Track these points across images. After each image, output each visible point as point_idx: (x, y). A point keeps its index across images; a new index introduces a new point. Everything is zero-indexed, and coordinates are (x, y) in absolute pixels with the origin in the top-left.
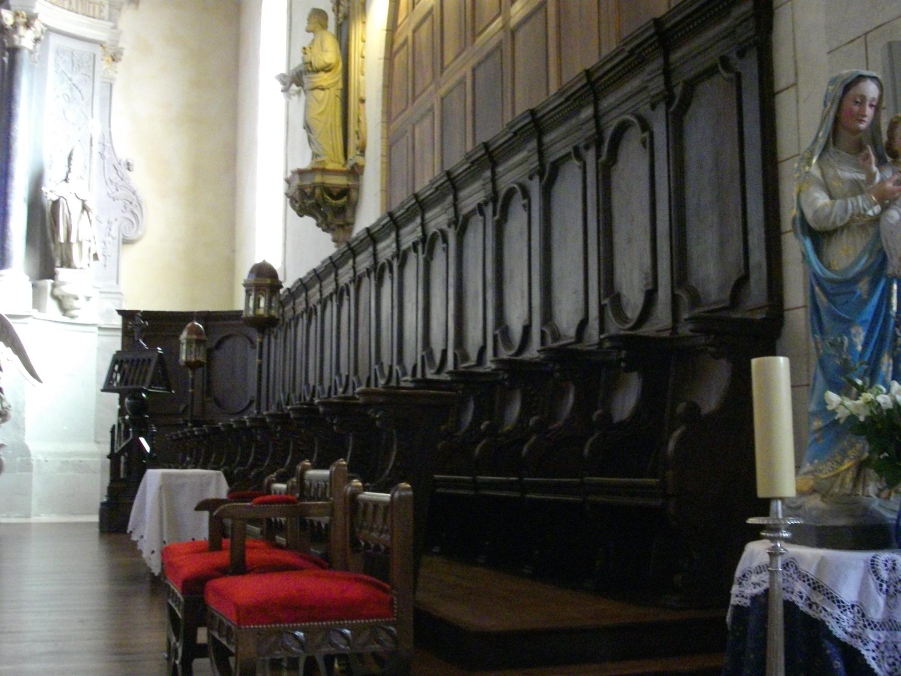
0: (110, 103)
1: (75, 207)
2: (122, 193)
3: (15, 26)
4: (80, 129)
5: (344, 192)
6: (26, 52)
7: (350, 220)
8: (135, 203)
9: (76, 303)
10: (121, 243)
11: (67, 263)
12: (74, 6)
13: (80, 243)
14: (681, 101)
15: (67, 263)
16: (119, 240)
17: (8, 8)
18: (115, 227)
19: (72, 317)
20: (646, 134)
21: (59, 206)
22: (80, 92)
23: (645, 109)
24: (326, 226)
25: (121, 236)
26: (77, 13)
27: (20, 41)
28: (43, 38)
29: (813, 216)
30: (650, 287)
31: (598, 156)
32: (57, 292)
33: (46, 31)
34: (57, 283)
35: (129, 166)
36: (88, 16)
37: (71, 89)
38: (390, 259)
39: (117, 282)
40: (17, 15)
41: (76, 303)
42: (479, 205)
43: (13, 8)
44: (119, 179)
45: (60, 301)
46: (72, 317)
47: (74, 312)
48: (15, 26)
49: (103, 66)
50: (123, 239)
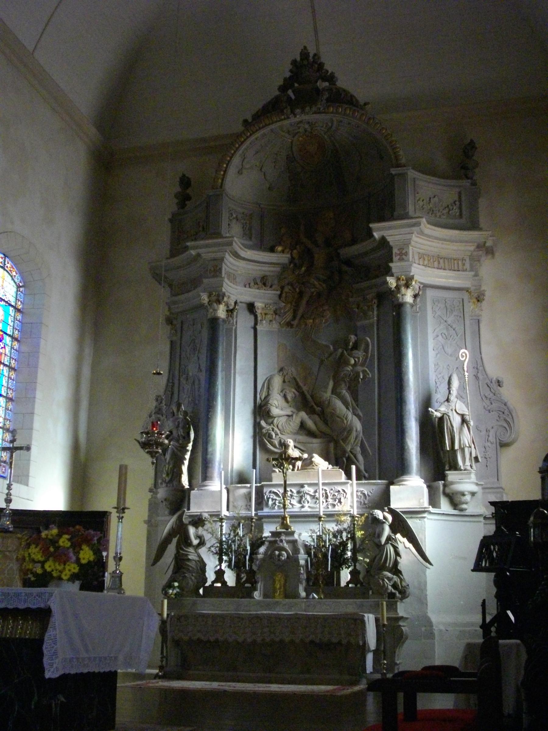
1: (456, 421)
6: (408, 306)
8: (506, 412)
11: (455, 467)
13: (462, 450)
15: (455, 467)
17: (392, 275)
18: (492, 433)
25: (498, 441)
26: (444, 269)
27: (403, 298)
32: (448, 490)
35: (499, 383)
37: (447, 329)
40: (398, 279)
43: (395, 275)
44: (492, 395)
46: (462, 510)
47: (464, 506)
49: (470, 307)
50: (500, 443)
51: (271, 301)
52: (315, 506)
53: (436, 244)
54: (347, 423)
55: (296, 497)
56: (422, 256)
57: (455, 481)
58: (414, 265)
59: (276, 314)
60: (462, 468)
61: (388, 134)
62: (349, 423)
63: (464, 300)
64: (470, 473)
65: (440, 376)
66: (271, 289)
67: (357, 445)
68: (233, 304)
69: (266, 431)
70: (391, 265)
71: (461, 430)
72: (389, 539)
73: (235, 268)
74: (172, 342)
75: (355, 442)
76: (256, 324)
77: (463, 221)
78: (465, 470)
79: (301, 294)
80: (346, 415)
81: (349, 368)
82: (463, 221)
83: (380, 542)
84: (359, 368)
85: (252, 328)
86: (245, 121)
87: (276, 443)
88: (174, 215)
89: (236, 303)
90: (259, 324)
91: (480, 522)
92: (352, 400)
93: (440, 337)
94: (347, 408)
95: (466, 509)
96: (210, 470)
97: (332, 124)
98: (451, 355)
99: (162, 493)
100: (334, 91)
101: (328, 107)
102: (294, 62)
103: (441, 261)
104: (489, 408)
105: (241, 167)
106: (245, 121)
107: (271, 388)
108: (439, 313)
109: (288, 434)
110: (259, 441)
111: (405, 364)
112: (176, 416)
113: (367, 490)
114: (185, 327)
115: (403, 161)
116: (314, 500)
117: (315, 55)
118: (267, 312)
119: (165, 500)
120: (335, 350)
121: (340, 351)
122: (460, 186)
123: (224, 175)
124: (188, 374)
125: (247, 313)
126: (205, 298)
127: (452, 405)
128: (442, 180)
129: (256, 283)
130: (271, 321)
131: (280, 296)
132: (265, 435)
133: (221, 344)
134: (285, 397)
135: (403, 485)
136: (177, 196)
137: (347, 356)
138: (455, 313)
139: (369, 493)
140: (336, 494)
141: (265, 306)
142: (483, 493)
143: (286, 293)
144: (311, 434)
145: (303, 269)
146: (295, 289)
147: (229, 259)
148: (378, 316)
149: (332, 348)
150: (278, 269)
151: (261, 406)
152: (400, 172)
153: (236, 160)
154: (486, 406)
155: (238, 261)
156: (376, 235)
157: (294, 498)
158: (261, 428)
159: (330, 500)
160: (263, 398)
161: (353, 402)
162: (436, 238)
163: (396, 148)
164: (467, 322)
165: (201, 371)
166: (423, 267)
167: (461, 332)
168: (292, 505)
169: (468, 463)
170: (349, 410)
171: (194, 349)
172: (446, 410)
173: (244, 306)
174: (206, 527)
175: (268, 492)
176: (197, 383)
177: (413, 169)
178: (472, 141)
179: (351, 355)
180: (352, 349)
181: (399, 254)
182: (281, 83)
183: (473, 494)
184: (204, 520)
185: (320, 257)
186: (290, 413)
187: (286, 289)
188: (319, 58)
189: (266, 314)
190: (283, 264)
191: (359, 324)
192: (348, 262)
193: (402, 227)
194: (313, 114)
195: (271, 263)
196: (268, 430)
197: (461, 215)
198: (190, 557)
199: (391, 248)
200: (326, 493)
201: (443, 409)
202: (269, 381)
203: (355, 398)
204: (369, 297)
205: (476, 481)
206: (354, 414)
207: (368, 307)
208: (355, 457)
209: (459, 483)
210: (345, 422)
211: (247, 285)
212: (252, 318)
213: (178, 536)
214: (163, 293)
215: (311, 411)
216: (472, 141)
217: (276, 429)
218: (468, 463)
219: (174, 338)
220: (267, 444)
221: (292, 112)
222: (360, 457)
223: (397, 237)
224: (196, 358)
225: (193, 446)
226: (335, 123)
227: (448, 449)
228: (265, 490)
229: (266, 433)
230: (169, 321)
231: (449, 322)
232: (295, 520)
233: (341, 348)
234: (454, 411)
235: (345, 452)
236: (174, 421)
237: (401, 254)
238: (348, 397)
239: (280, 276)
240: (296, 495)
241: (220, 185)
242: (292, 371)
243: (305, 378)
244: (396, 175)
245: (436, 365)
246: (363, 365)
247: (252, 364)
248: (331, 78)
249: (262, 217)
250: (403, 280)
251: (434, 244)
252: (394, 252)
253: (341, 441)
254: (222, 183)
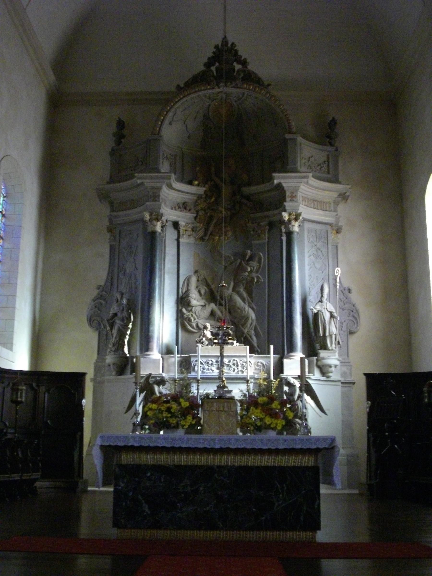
0: (337, 255)
1: (327, 316)
2: (347, 306)
3: (289, 221)
4: (322, 272)
6: (296, 233)
8: (354, 311)
9: (331, 369)
10: (348, 333)
11: (324, 347)
12: (316, 206)
13: (331, 336)
15: (324, 347)
16: (347, 333)
17: (285, 211)
18: (345, 324)
21: (318, 316)
22: (321, 252)
25: (348, 330)
26: (318, 209)
27: (293, 228)
28: (301, 224)
29: (243, 59)
32: (319, 363)
33: (303, 220)
34: (319, 358)
35: (349, 291)
36: (323, 210)
37: (317, 251)
39: (348, 356)
40: (290, 214)
41: (331, 369)
43: (287, 211)
44: (345, 298)
46: (328, 377)
48: (289, 221)
49: (332, 236)
50: (350, 332)
51: (190, 222)
52: (229, 371)
53: (315, 191)
54: (245, 312)
55: (215, 365)
56: (304, 199)
57: (325, 357)
58: (301, 205)
59: (193, 231)
60: (330, 348)
61: (284, 109)
62: (246, 313)
63: (328, 231)
64: (335, 352)
65: (311, 284)
66: (189, 212)
67: (252, 329)
68: (165, 222)
69: (187, 316)
70: (285, 203)
71: (330, 323)
72: (299, 397)
73: (166, 195)
74: (111, 246)
75: (250, 327)
78: (332, 350)
79: (211, 218)
80: (244, 307)
81: (247, 274)
83: (294, 399)
84: (254, 275)
85: (176, 240)
86: (178, 86)
87: (194, 325)
88: (113, 150)
89: (167, 221)
90: (181, 237)
91: (339, 385)
92: (248, 296)
93: (312, 256)
94: (245, 303)
95: (331, 377)
96: (151, 344)
97: (243, 96)
98: (319, 270)
99: (110, 359)
100: (247, 72)
102: (216, 47)
104: (343, 307)
105: (171, 120)
106: (178, 86)
107: (190, 285)
108: (311, 239)
109: (203, 319)
110: (181, 323)
111: (294, 275)
112: (119, 302)
113: (265, 361)
115: (294, 130)
116: (229, 368)
118: (187, 229)
119: (114, 364)
120: (235, 260)
121: (239, 261)
124: (125, 271)
126: (147, 216)
127: (324, 304)
129: (179, 207)
130: (189, 236)
131: (196, 218)
133: (158, 251)
134: (199, 292)
135: (292, 359)
136: (114, 135)
137: (245, 265)
138: (322, 240)
139: (267, 364)
140: (244, 364)
141: (186, 225)
142: (341, 366)
143: (200, 216)
146: (207, 214)
147: (165, 189)
148: (268, 238)
149: (232, 258)
150: (195, 198)
151: (182, 298)
152: (292, 137)
153: (170, 114)
154: (341, 306)
155: (168, 190)
156: (276, 182)
157: (213, 366)
158: (183, 314)
159: (240, 368)
160: (184, 292)
161: (249, 299)
162: (317, 188)
163: (290, 120)
164: (330, 246)
165: (137, 269)
166: (305, 207)
167: (325, 254)
168: (213, 371)
169: (334, 345)
170: (246, 304)
172: (321, 308)
173: (171, 223)
174: (165, 386)
175: (195, 360)
177: (301, 136)
178: (333, 118)
179: (248, 265)
180: (248, 260)
181: (291, 197)
182: (206, 61)
183: (336, 366)
184: (166, 381)
186: (203, 304)
187: (200, 213)
188: (235, 46)
189: (186, 230)
190: (199, 195)
191: (253, 242)
192: (248, 198)
193: (295, 177)
194: (232, 87)
195: (187, 193)
196: (188, 315)
199: (285, 192)
200: (237, 363)
201: (318, 307)
204: (262, 224)
205: (338, 358)
206: (250, 306)
207: (261, 231)
208: (251, 337)
209: (329, 359)
210: (244, 312)
212: (176, 232)
213: (145, 392)
216: (333, 118)
217: (194, 315)
219: (114, 243)
220: (187, 326)
223: (290, 185)
224: (133, 260)
225: (132, 325)
226: (245, 95)
227: (321, 335)
228: (192, 359)
229: (187, 318)
230: (110, 230)
231: (318, 246)
232: (231, 381)
233: (240, 259)
234: (326, 309)
235: (243, 333)
236: (118, 306)
238: (245, 295)
239: (196, 203)
240: (215, 363)
242: (203, 273)
243: (213, 279)
245: (310, 276)
246: (257, 272)
247: (176, 266)
248: (244, 63)
249: (183, 158)
250: (293, 215)
251: (313, 191)
252: (287, 195)
253: (241, 327)
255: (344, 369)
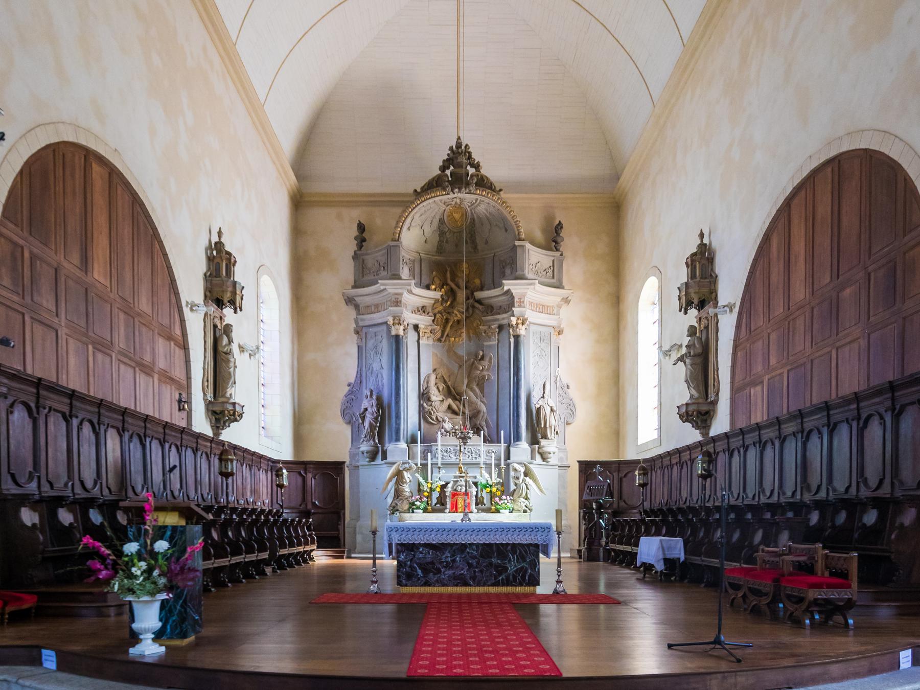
1: (548, 410)
5: (707, 413)
6: (522, 337)
7: (709, 425)
9: (549, 456)
11: (545, 437)
13: (551, 427)
14: (899, 411)
15: (545, 437)
19: (547, 462)
20: (882, 421)
23: (882, 410)
24: (696, 426)
30: (881, 477)
31: (858, 424)
32: (540, 451)
38: (739, 447)
41: (549, 456)
42: (794, 433)
45: (541, 454)
46: (547, 462)
47: (549, 460)
59: (431, 333)
71: (550, 415)
74: (358, 346)
76: (419, 339)
77: (554, 281)
79: (447, 321)
82: (554, 281)
87: (434, 418)
94: (477, 398)
101: (476, 189)
102: (451, 149)
103: (541, 307)
106: (415, 191)
114: (369, 337)
117: (467, 145)
121: (472, 360)
122: (554, 256)
123: (400, 231)
125: (413, 331)
128: (544, 251)
132: (427, 412)
134: (438, 388)
136: (356, 238)
142: (559, 452)
144: (455, 413)
145: (449, 303)
146: (443, 317)
151: (423, 394)
158: (424, 408)
163: (519, 226)
166: (531, 311)
169: (553, 435)
171: (377, 353)
176: (380, 375)
180: (480, 360)
185: (462, 295)
186: (441, 399)
187: (438, 316)
192: (479, 301)
197: (553, 277)
198: (406, 490)
199: (513, 297)
201: (541, 403)
202: (428, 378)
203: (482, 391)
211: (414, 312)
214: (352, 313)
215: (454, 399)
217: (434, 409)
218: (553, 435)
221: (452, 191)
222: (485, 428)
226: (478, 201)
230: (357, 332)
237: (520, 302)
241: (397, 238)
243: (449, 376)
244: (518, 246)
247: (417, 366)
248: (477, 167)
254: (399, 237)
255: (562, 455)
